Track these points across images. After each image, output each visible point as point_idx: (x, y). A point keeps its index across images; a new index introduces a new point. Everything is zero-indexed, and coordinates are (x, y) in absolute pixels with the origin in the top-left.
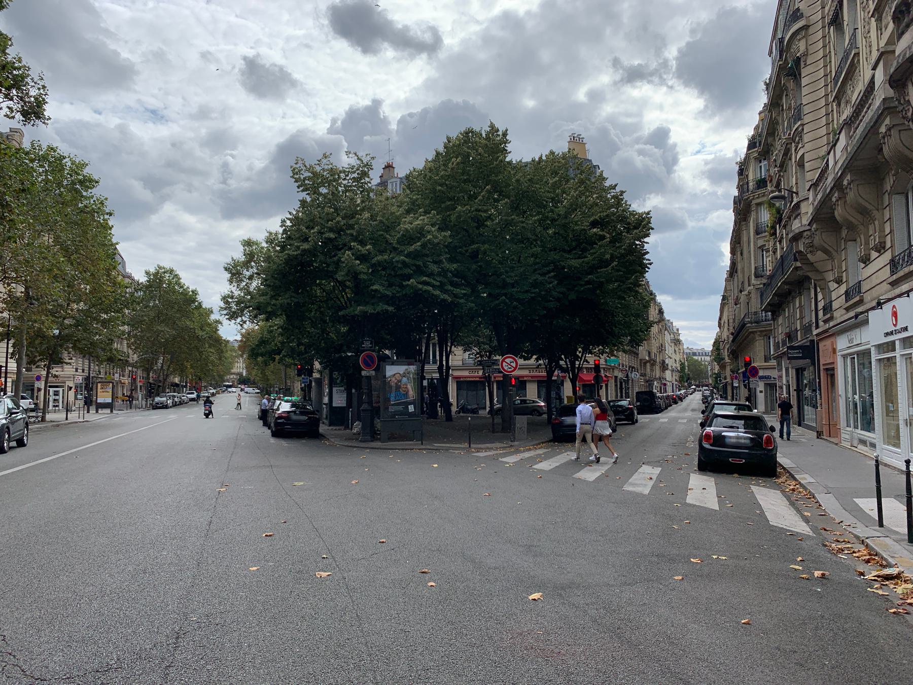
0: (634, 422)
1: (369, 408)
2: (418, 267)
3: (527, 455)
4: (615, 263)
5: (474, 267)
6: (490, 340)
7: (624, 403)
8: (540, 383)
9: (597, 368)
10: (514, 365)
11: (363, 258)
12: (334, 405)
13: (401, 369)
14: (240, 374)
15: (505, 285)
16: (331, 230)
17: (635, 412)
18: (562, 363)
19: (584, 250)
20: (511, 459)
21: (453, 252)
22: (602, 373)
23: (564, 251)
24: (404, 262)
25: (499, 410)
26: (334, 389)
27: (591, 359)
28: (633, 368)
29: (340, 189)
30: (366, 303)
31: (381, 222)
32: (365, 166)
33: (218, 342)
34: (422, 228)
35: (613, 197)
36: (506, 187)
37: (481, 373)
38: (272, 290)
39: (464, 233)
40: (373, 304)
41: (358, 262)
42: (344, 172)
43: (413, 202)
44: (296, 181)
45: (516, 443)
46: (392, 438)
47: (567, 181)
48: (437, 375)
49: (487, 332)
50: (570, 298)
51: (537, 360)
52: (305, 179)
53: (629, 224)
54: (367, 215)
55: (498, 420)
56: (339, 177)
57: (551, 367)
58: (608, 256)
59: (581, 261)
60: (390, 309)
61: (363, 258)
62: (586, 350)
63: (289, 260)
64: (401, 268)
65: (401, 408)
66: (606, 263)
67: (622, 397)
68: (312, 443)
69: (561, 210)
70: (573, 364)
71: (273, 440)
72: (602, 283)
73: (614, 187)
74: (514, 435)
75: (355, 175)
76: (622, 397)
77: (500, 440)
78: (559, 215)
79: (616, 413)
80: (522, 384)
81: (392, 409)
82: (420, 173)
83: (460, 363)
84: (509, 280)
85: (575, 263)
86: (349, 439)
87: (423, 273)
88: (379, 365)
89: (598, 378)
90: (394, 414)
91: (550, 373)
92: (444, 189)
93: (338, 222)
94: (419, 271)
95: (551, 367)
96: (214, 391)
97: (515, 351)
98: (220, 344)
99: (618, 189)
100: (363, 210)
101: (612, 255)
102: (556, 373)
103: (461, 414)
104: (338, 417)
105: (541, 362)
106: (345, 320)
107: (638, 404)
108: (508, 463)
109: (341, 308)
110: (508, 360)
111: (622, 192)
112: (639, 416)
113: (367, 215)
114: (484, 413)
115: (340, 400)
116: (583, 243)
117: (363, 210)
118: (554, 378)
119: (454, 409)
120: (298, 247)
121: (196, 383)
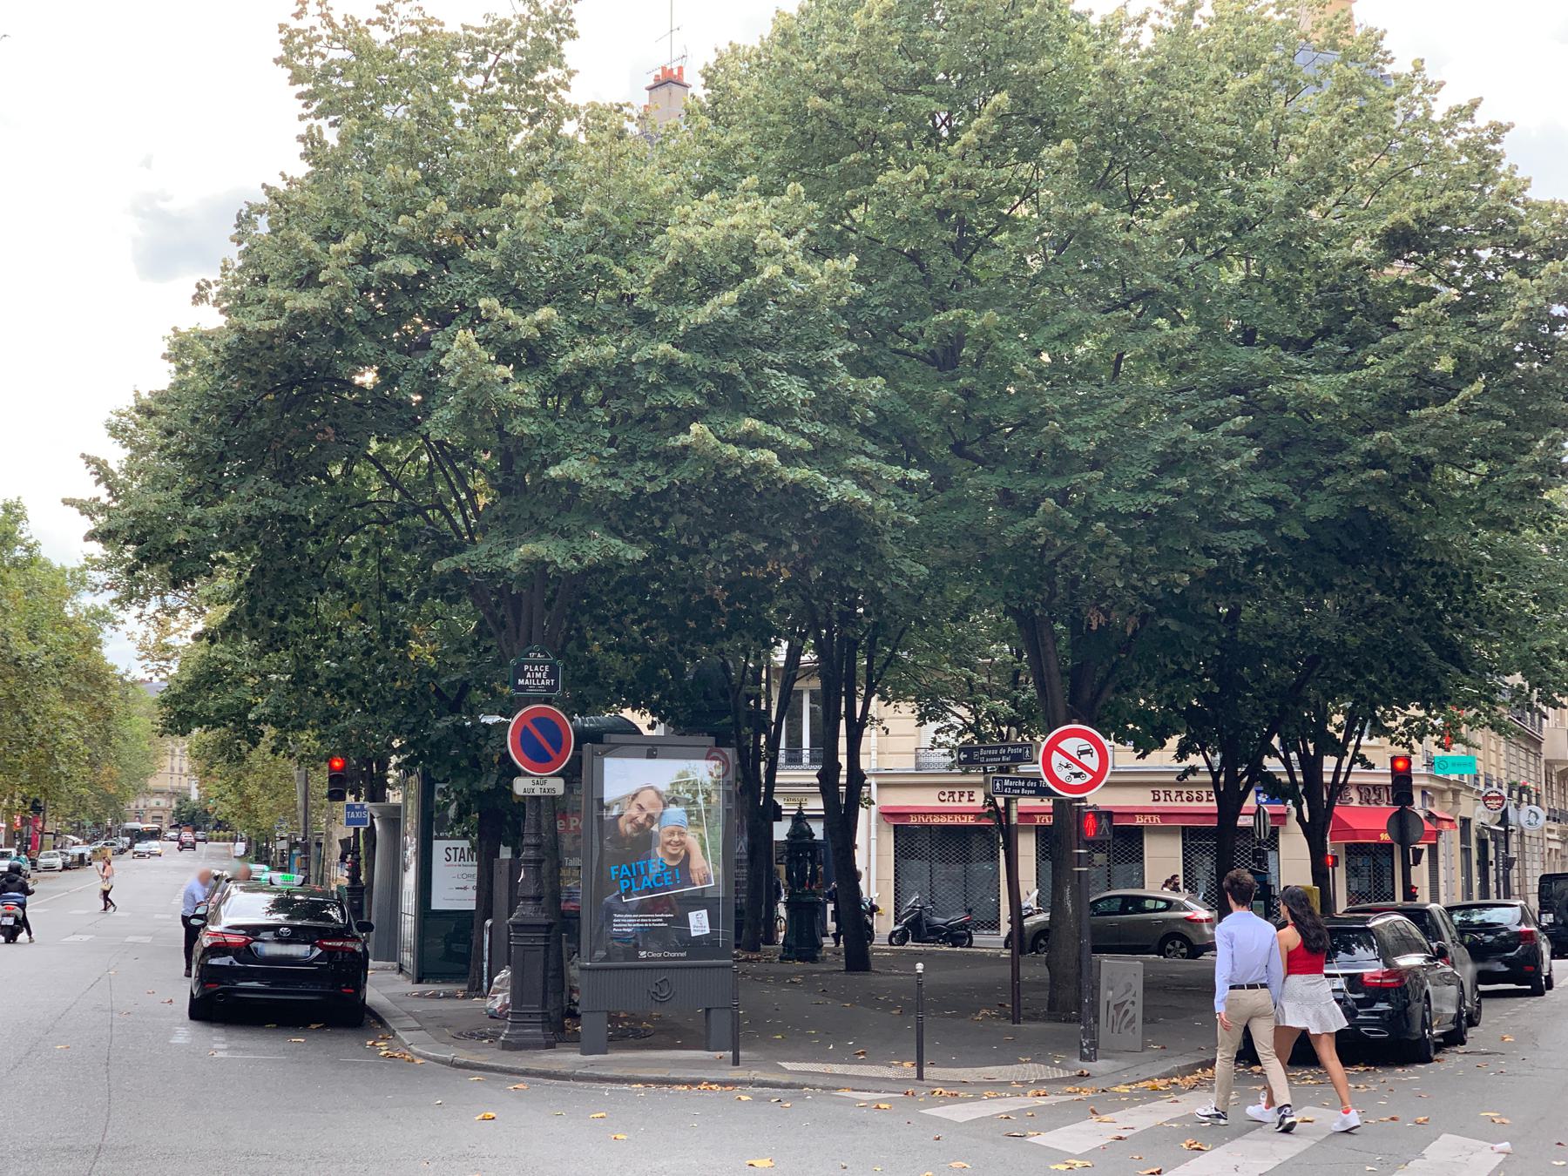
0: (1538, 985)
1: (542, 919)
2: (728, 381)
3: (1141, 1118)
4: (1479, 386)
5: (944, 392)
6: (1015, 682)
7: (1506, 917)
8: (1192, 837)
9: (1402, 783)
10: (1092, 762)
11: (527, 355)
12: (437, 904)
13: (662, 773)
14: (183, 798)
15: (1064, 460)
16: (406, 246)
17: (1545, 948)
18: (1272, 764)
19: (1358, 340)
20: (1079, 1138)
21: (876, 342)
22: (1418, 805)
23: (1287, 343)
24: (670, 367)
25: (1042, 932)
26: (439, 847)
27: (1379, 752)
28: (1523, 789)
29: (457, 107)
30: (538, 528)
31: (596, 220)
32: (546, 24)
33: (92, 682)
34: (748, 245)
35: (1463, 147)
36: (1066, 100)
37: (979, 799)
38: (190, 470)
39: (908, 267)
40: (565, 534)
41: (507, 371)
42: (471, 42)
43: (725, 158)
44: (296, 79)
45: (1100, 1066)
46: (630, 1032)
47: (1294, 90)
48: (816, 805)
49: (1002, 651)
50: (1313, 512)
51: (1182, 753)
52: (327, 72)
53: (1524, 243)
54: (541, 193)
55: (1035, 970)
56: (453, 66)
57: (1233, 779)
58: (1445, 364)
59: (1345, 378)
60: (636, 554)
61: (527, 355)
62: (1364, 718)
63: (243, 355)
64: (657, 387)
65: (658, 920)
66: (1444, 389)
67: (1485, 892)
68: (343, 1046)
69: (1273, 187)
70: (1312, 767)
71: (186, 1033)
72: (1426, 465)
73: (1467, 112)
74: (1092, 1034)
75: (511, 57)
76: (1485, 892)
77: (1040, 1051)
78: (1264, 206)
79: (1478, 952)
80: (1126, 839)
81: (626, 924)
82: (758, 60)
83: (908, 764)
84: (1074, 443)
85: (1323, 386)
86: (474, 1035)
87: (742, 405)
88: (577, 761)
89: (1403, 822)
90: (631, 945)
91: (1230, 801)
92: (835, 105)
93: (435, 220)
94: (729, 397)
95: (1233, 779)
96: (87, 850)
97: (1107, 719)
98: (104, 689)
99: (1482, 118)
100: (531, 175)
101: (1461, 356)
102: (1250, 802)
103: (910, 945)
104: (449, 950)
105: (1196, 760)
106: (453, 587)
107: (1548, 918)
108: (1062, 1156)
109: (447, 547)
110: (1071, 745)
111: (1498, 130)
112: (1558, 964)
113: (541, 193)
114: (992, 942)
115: (455, 888)
116: (1348, 317)
117: (531, 175)
118: (1244, 821)
119: (884, 925)
120: (279, 306)
121: (24, 821)
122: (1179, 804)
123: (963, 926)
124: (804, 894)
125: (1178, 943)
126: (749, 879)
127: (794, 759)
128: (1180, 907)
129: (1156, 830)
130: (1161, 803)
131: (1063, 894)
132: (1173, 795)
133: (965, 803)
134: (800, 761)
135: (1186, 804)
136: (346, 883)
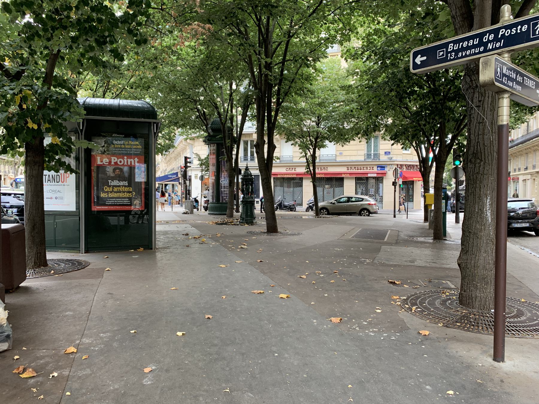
123: (294, 205)
124: (249, 198)
125: (365, 211)
126: (229, 192)
128: (363, 200)
129: (348, 178)
130: (349, 171)
132: (369, 168)
133: (293, 171)
135: (357, 171)
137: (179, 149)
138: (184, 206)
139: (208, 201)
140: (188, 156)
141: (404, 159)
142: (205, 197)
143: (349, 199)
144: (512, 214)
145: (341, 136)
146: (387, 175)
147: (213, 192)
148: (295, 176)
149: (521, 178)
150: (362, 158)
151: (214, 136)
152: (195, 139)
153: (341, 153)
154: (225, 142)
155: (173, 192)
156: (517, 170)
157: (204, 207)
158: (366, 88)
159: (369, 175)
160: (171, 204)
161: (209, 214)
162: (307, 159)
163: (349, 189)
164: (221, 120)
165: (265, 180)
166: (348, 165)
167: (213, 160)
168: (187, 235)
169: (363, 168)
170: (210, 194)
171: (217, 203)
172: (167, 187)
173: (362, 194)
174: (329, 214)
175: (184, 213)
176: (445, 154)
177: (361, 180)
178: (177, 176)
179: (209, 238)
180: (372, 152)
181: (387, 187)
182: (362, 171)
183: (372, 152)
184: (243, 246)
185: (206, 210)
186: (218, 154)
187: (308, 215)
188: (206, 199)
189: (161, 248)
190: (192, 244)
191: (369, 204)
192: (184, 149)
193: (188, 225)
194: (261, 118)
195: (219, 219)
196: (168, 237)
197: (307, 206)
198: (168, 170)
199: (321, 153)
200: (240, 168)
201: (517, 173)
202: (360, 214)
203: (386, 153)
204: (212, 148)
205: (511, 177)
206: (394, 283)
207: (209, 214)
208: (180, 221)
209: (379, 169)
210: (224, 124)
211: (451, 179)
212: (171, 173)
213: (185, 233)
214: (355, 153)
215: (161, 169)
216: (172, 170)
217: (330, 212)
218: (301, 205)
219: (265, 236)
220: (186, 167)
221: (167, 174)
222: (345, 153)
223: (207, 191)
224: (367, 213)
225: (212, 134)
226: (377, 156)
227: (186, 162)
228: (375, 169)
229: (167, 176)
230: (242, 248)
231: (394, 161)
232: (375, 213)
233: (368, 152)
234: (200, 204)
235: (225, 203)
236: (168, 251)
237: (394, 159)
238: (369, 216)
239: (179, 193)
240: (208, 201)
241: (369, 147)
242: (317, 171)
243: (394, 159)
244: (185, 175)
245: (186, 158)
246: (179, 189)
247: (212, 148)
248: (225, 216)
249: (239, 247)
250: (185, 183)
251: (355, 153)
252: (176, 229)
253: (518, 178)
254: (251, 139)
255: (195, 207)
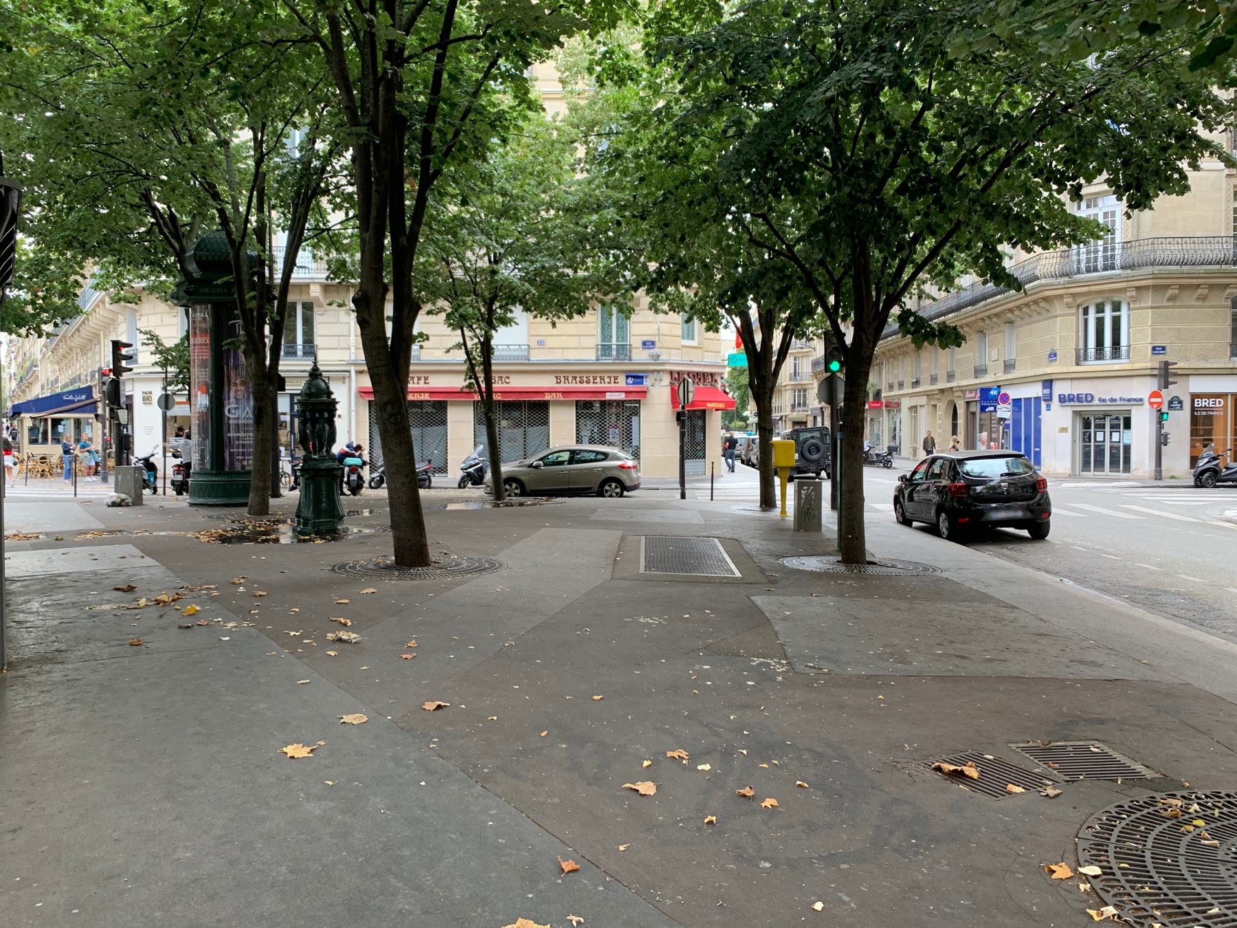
122: (574, 385)
124: (322, 460)
125: (614, 485)
127: (292, 353)
128: (606, 456)
129: (558, 403)
130: (562, 385)
131: (773, 486)
132: (607, 380)
133: (422, 384)
134: (295, 354)
135: (579, 385)
136: (300, 253)
137: (93, 321)
138: (112, 479)
139: (188, 466)
140: (124, 340)
141: (686, 359)
142: (175, 456)
143: (574, 456)
144: (979, 489)
145: (556, 298)
146: (648, 395)
147: (201, 444)
148: (426, 397)
149: (906, 403)
150: (591, 356)
151: (205, 282)
152: (144, 295)
153: (540, 343)
154: (241, 296)
155: (77, 441)
156: (896, 386)
157: (173, 483)
158: (661, 158)
159: (609, 397)
160: (72, 475)
161: (192, 505)
162: (467, 353)
163: (562, 431)
164: (229, 233)
165: (389, 408)
166: (558, 370)
167: (200, 352)
168: (131, 589)
169: (595, 378)
170: (194, 450)
171: (217, 474)
172: (60, 429)
173: (592, 441)
174: (524, 493)
175: (114, 504)
176: (871, 338)
177: (591, 409)
178: (90, 396)
179: (213, 599)
180: (614, 341)
181: (657, 426)
182: (591, 385)
183: (614, 341)
184: (344, 635)
185: (179, 493)
186: (220, 333)
187: (467, 500)
188: (178, 461)
189: (29, 662)
190: (151, 632)
191: (622, 467)
192: (111, 324)
193: (129, 549)
194: (373, 213)
195: (227, 520)
196: (57, 605)
197: (461, 474)
198: (64, 379)
199: (502, 338)
200: (282, 374)
201: (896, 392)
202: (600, 494)
203: (644, 343)
204: (199, 316)
205: (883, 401)
206: (958, 775)
207: (192, 505)
208: (101, 532)
209: (630, 381)
210: (237, 246)
211: (744, 405)
212: (71, 388)
213: (131, 638)
214: (573, 342)
215: (42, 380)
216: (73, 381)
217: (528, 489)
218: (443, 469)
219: (395, 584)
220: (118, 370)
221: (59, 391)
222: (550, 342)
223: (182, 441)
224: (618, 490)
225: (197, 274)
226: (624, 349)
227: (117, 357)
228: (622, 382)
229: (59, 395)
230: (340, 640)
231: (664, 364)
232: (636, 487)
233: (603, 340)
234: (160, 474)
235: (238, 473)
236: (57, 673)
237: (663, 358)
238: (621, 496)
239: (97, 445)
240: (188, 466)
241: (606, 328)
242: (496, 386)
243: (663, 358)
244: (114, 394)
245: (117, 345)
246: (96, 433)
247: (199, 316)
248: (246, 509)
249: (330, 636)
250: (114, 415)
251: (573, 342)
252: (89, 566)
253: (898, 404)
254: (305, 298)
255: (146, 484)
